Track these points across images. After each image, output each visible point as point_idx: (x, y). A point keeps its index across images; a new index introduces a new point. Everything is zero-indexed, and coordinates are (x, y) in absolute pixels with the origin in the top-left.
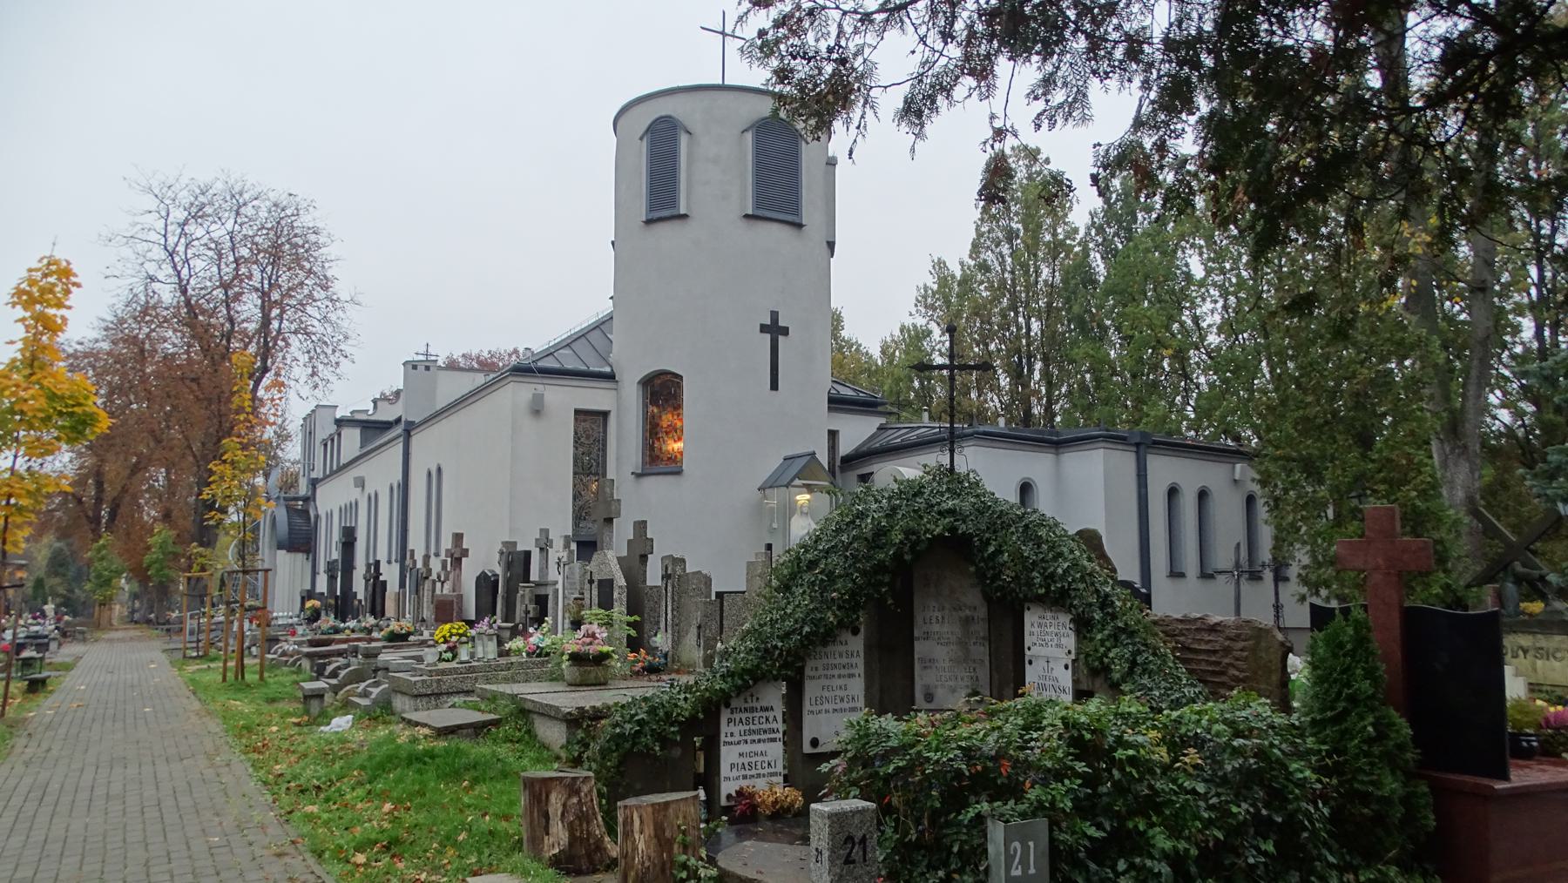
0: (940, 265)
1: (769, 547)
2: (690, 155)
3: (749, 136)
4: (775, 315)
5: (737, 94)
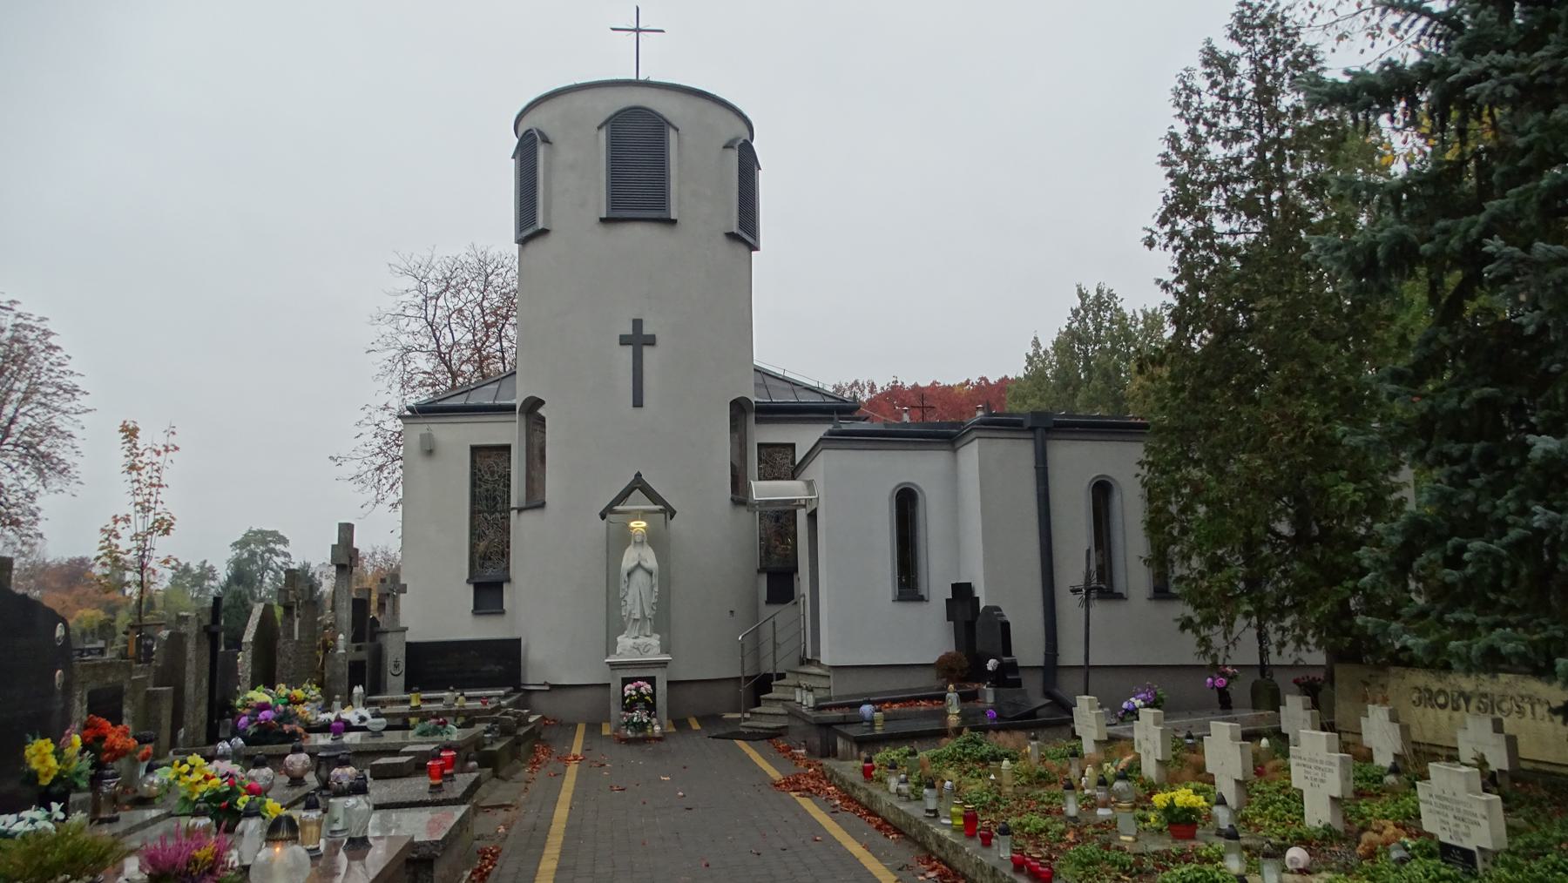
0: (642, 167)
1: (130, 433)
2: (548, 164)
3: (603, 134)
4: (637, 324)
5: (596, 90)
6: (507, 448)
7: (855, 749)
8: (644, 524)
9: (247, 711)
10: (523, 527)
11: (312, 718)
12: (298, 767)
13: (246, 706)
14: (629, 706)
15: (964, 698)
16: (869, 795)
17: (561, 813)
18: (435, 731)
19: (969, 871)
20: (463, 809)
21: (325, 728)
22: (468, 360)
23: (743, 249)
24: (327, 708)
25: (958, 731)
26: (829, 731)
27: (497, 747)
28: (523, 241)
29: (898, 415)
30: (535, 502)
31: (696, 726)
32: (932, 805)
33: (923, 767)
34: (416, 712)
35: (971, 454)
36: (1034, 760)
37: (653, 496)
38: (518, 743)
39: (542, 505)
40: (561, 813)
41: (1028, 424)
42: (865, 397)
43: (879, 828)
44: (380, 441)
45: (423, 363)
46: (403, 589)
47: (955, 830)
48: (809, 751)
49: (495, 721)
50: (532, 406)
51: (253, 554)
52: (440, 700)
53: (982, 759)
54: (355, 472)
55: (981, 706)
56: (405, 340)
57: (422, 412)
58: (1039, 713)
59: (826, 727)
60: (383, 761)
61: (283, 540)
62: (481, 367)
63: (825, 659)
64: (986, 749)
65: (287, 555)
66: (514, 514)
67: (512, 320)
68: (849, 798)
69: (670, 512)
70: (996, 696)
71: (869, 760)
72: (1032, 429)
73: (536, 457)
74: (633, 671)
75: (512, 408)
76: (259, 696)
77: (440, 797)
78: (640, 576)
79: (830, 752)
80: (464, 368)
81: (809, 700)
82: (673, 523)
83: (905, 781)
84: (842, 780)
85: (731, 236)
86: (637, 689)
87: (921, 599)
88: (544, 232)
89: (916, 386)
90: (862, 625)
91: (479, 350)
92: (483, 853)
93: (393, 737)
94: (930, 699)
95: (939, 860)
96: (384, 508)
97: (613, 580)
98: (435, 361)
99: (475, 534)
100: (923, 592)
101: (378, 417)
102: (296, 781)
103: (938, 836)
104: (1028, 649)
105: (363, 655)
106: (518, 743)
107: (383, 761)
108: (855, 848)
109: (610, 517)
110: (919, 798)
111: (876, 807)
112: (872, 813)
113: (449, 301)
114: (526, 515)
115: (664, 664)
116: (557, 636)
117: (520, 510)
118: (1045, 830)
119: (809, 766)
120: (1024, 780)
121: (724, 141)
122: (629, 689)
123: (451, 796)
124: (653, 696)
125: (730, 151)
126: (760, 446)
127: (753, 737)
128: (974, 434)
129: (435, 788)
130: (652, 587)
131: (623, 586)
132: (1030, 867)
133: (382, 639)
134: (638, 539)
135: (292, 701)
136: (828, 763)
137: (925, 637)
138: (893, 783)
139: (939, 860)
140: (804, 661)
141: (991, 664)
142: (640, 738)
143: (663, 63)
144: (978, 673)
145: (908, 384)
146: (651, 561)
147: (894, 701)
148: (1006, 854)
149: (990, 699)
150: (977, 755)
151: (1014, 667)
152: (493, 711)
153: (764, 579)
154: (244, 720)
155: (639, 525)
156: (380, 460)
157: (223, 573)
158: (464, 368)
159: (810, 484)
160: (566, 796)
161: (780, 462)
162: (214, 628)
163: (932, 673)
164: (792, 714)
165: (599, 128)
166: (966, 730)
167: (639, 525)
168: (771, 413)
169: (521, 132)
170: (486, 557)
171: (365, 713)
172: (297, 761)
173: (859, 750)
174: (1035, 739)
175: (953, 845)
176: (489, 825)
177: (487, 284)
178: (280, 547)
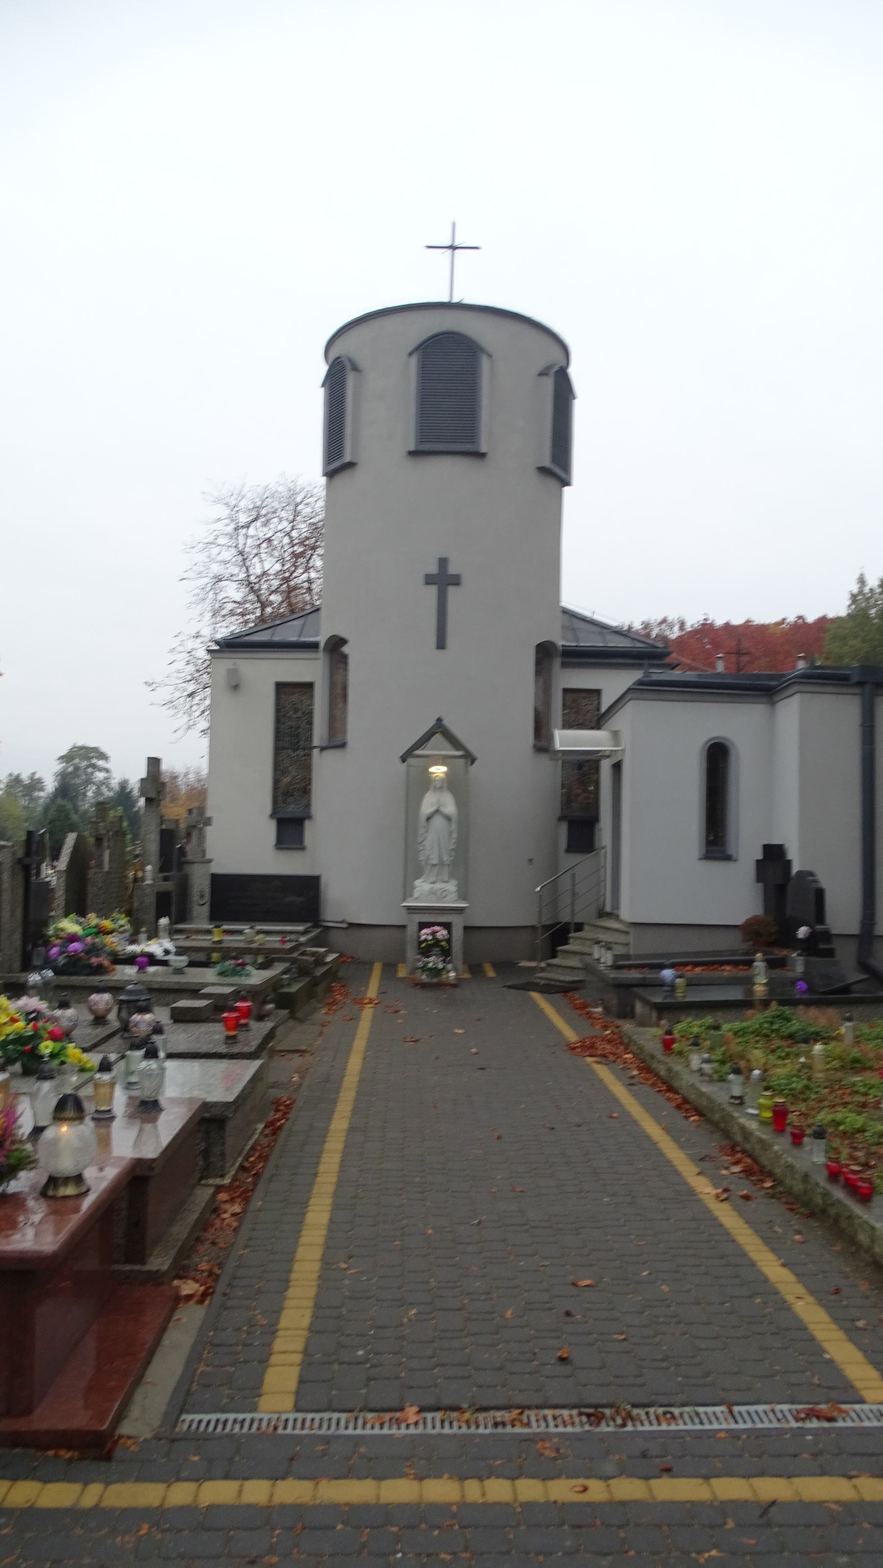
0: (455, 395)
3: (414, 362)
6: (310, 686)
7: (654, 1015)
8: (444, 769)
9: (58, 941)
10: (326, 768)
11: (119, 948)
12: (102, 1006)
13: (58, 937)
14: (426, 950)
15: (773, 964)
16: (669, 1070)
17: (355, 1063)
18: (234, 973)
19: (778, 1171)
20: (257, 1063)
21: (131, 960)
22: (275, 591)
23: (553, 483)
24: (133, 941)
25: (766, 1004)
26: (628, 992)
27: (294, 988)
28: (331, 474)
29: (713, 665)
30: (337, 742)
31: (491, 973)
32: (737, 1092)
33: (727, 1043)
34: (217, 947)
35: (791, 710)
36: (849, 1039)
37: (455, 743)
38: (314, 983)
39: (343, 746)
40: (355, 1063)
41: (856, 678)
42: (675, 634)
43: (678, 1107)
44: (191, 668)
45: (234, 592)
46: (208, 822)
47: (763, 1123)
48: (607, 1010)
49: (294, 961)
50: (336, 645)
51: (77, 769)
52: (240, 932)
53: (791, 1036)
54: (168, 698)
55: (790, 975)
56: (216, 569)
57: (230, 646)
58: (854, 987)
59: (624, 987)
60: (183, 1003)
61: (103, 756)
62: (288, 597)
63: (627, 913)
64: (795, 1026)
65: (107, 771)
66: (316, 752)
67: (320, 551)
68: (646, 1069)
69: (470, 758)
70: (807, 965)
71: (669, 1032)
72: (860, 684)
73: (339, 695)
74: (428, 917)
75: (314, 646)
76: (70, 926)
77: (236, 1049)
78: (438, 821)
79: (627, 1013)
80: (273, 598)
81: (608, 958)
82: (473, 768)
83: (708, 1061)
84: (641, 1048)
85: (543, 471)
86: (434, 933)
87: (728, 858)
88: (351, 465)
89: (727, 626)
90: (664, 879)
91: (287, 580)
92: (277, 1104)
93: (196, 976)
94: (735, 964)
95: (744, 1151)
96: (195, 733)
97: (411, 826)
98: (244, 590)
99: (279, 769)
100: (731, 851)
101: (191, 644)
102: (99, 1020)
103: (743, 1129)
104: (842, 913)
105: (169, 886)
106: (314, 983)
107: (183, 1003)
108: (653, 1130)
109: (411, 760)
110: (722, 1079)
111: (676, 1084)
112: (671, 1089)
113: (257, 531)
114: (328, 754)
115: (460, 910)
116: (358, 873)
117: (323, 749)
118: (862, 1130)
119: (605, 1027)
120: (836, 1063)
121: (540, 367)
122: (425, 933)
123: (247, 1049)
124: (449, 941)
125: (545, 378)
126: (566, 691)
127: (548, 989)
128: (796, 688)
129: (231, 1040)
130: (451, 833)
131: (421, 831)
132: (847, 1180)
133: (188, 869)
134: (438, 784)
135: (101, 931)
136: (627, 1026)
137: (730, 897)
138: (695, 1060)
139: (744, 1151)
140: (602, 914)
141: (802, 932)
142: (435, 984)
143: (479, 284)
144: (787, 939)
145: (719, 622)
146: (450, 807)
147: (696, 964)
148: (819, 1158)
149: (800, 968)
150: (785, 1031)
151: (827, 936)
152: (292, 950)
153: (563, 829)
154: (54, 950)
155: (439, 770)
156: (191, 687)
157: (50, 785)
158: (273, 598)
159: (615, 734)
160: (360, 1043)
161: (585, 710)
162: (27, 861)
163: (738, 936)
164: (588, 969)
165: (410, 354)
166: (774, 1004)
167: (439, 770)
168: (578, 657)
169: (332, 357)
170: (288, 794)
171: (168, 944)
172: (102, 999)
173: (660, 1018)
174: (849, 1019)
175: (761, 1141)
176: (286, 1070)
177: (296, 514)
178: (101, 763)
